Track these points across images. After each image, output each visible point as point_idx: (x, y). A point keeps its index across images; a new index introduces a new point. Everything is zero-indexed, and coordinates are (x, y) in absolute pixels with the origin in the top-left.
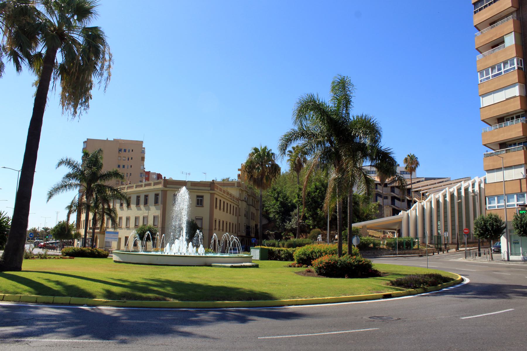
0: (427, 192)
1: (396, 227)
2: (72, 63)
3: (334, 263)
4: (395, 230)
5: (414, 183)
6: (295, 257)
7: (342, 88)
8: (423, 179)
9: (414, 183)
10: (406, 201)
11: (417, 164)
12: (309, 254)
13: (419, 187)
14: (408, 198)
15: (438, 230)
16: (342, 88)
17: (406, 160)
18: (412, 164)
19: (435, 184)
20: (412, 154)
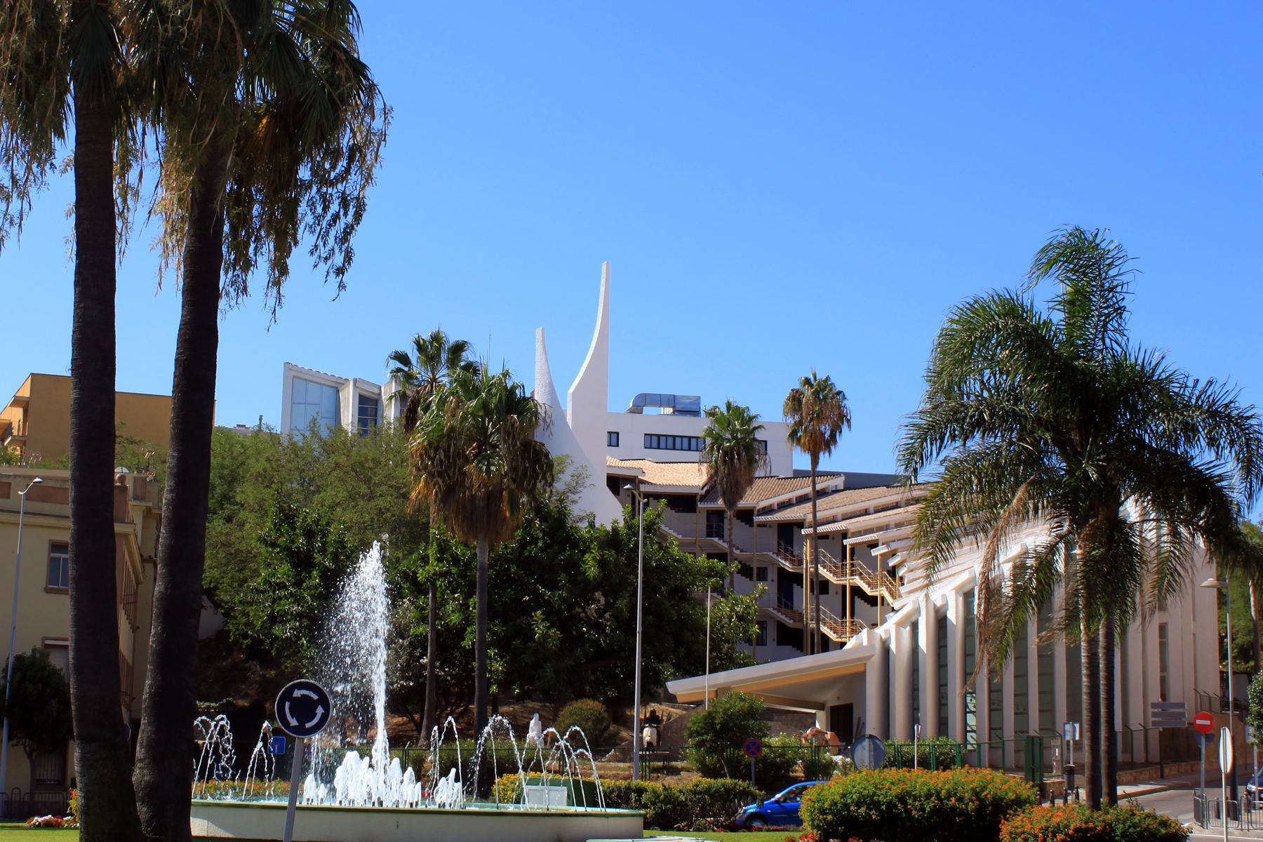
0: (874, 545)
1: (831, 698)
2: (268, 127)
3: (1104, 830)
4: (821, 706)
5: (802, 500)
6: (804, 814)
7: (1082, 260)
8: (839, 482)
9: (802, 500)
10: (772, 575)
11: (841, 419)
12: (890, 804)
13: (834, 521)
14: (788, 566)
15: (966, 713)
16: (1082, 260)
17: (795, 400)
18: (820, 417)
19: (896, 506)
20: (821, 376)
